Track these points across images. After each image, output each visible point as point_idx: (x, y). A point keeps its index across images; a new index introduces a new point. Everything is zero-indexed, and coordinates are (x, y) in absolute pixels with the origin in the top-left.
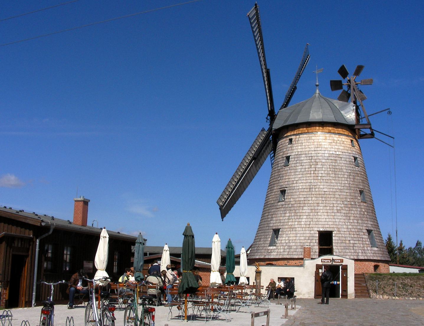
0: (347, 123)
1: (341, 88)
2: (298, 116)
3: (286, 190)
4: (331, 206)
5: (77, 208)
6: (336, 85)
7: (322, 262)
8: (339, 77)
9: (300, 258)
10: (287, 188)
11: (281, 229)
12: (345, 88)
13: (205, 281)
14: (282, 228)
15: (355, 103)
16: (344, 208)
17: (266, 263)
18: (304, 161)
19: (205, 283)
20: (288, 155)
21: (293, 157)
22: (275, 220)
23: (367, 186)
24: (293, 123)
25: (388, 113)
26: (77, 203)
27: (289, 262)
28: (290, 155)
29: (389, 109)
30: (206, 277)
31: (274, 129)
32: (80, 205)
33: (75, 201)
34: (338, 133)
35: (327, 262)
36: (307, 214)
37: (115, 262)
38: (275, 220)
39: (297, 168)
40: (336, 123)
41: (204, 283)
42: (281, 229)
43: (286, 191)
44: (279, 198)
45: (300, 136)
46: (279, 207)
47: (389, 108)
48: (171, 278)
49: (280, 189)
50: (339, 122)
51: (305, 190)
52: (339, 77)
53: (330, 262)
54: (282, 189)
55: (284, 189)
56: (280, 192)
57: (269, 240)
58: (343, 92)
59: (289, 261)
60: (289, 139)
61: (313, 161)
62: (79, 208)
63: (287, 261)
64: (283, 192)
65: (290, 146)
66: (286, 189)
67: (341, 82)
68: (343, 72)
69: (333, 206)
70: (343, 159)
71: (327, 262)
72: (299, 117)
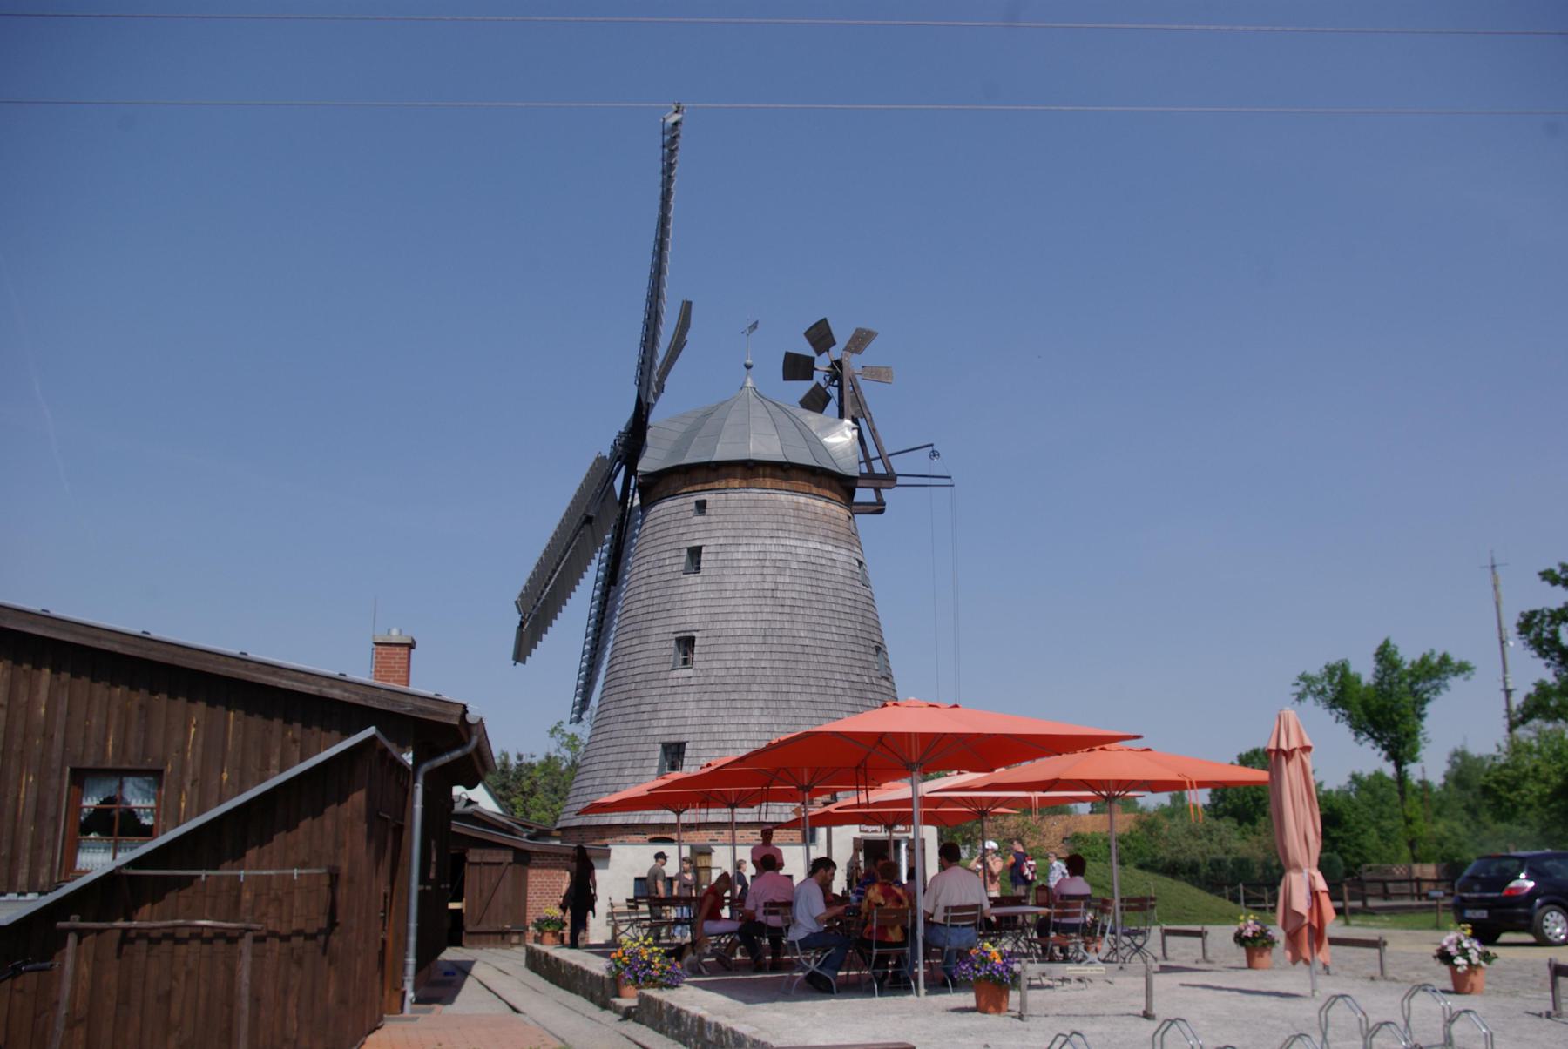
0: (837, 470)
1: (810, 378)
2: (717, 442)
3: (694, 637)
4: (820, 684)
5: (392, 667)
6: (797, 367)
7: (861, 831)
8: (807, 350)
9: (748, 823)
10: (697, 631)
11: (688, 742)
12: (819, 377)
13: (547, 893)
14: (692, 739)
15: (855, 420)
16: (849, 692)
17: (649, 837)
18: (743, 564)
19: (550, 897)
20: (697, 543)
21: (712, 549)
22: (667, 718)
23: (876, 631)
24: (706, 459)
25: (930, 456)
26: (384, 651)
27: (722, 833)
28: (701, 544)
29: (932, 445)
30: (551, 880)
31: (641, 472)
32: (394, 658)
33: (377, 644)
34: (787, 490)
35: (873, 832)
36: (762, 704)
37: (1089, 794)
38: (667, 718)
39: (726, 579)
40: (819, 468)
41: (544, 897)
42: (688, 742)
43: (697, 640)
44: (672, 657)
45: (730, 495)
46: (678, 682)
47: (930, 443)
48: (1118, 832)
49: (674, 633)
50: (792, 460)
51: (756, 640)
52: (807, 350)
53: (879, 830)
54: (682, 635)
55: (688, 634)
56: (674, 642)
57: (652, 772)
58: (813, 390)
59: (721, 831)
60: (697, 502)
61: (767, 563)
62: (394, 667)
63: (751, 831)
64: (686, 644)
65: (699, 519)
66: (695, 634)
67: (811, 360)
68: (821, 336)
69: (826, 686)
70: (838, 564)
71: (873, 832)
72: (718, 445)
